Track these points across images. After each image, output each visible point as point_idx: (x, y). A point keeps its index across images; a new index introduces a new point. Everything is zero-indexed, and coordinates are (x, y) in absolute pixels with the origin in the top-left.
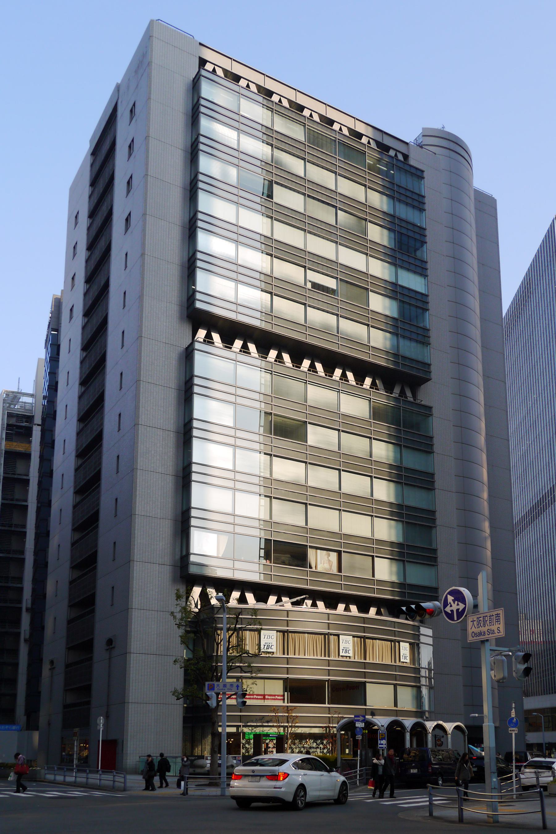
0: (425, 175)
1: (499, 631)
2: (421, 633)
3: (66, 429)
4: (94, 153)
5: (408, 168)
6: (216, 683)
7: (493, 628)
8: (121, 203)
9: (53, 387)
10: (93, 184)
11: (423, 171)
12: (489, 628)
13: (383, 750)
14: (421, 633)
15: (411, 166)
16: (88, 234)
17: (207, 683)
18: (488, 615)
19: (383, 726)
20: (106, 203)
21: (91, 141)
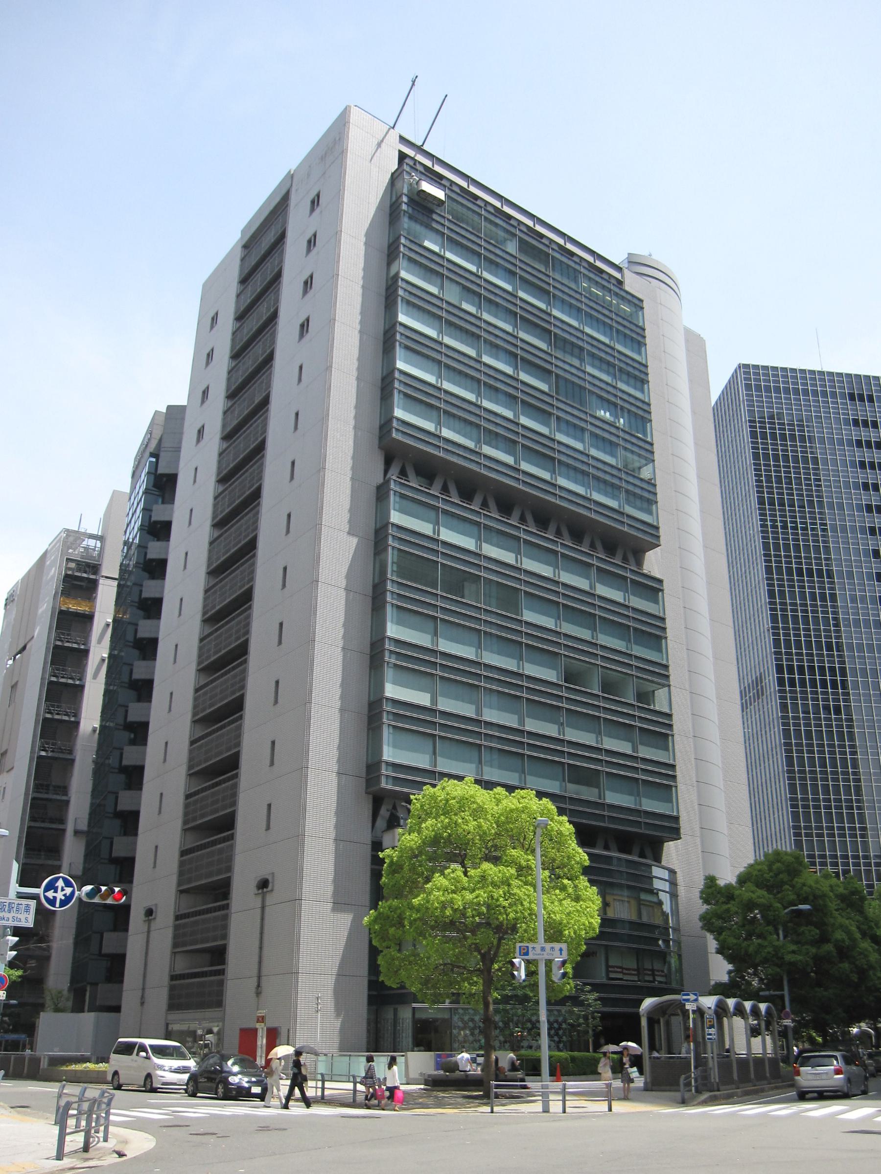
0: (645, 305)
1: (27, 921)
2: (654, 874)
3: (185, 588)
4: (248, 246)
5: (622, 293)
6: (531, 945)
7: (19, 916)
8: (290, 304)
9: (157, 530)
10: (244, 281)
11: (641, 301)
12: (16, 915)
13: (712, 1043)
14: (654, 874)
15: (627, 292)
16: (233, 340)
17: (518, 945)
18: (17, 902)
19: (710, 1008)
20: (265, 304)
21: (243, 232)
